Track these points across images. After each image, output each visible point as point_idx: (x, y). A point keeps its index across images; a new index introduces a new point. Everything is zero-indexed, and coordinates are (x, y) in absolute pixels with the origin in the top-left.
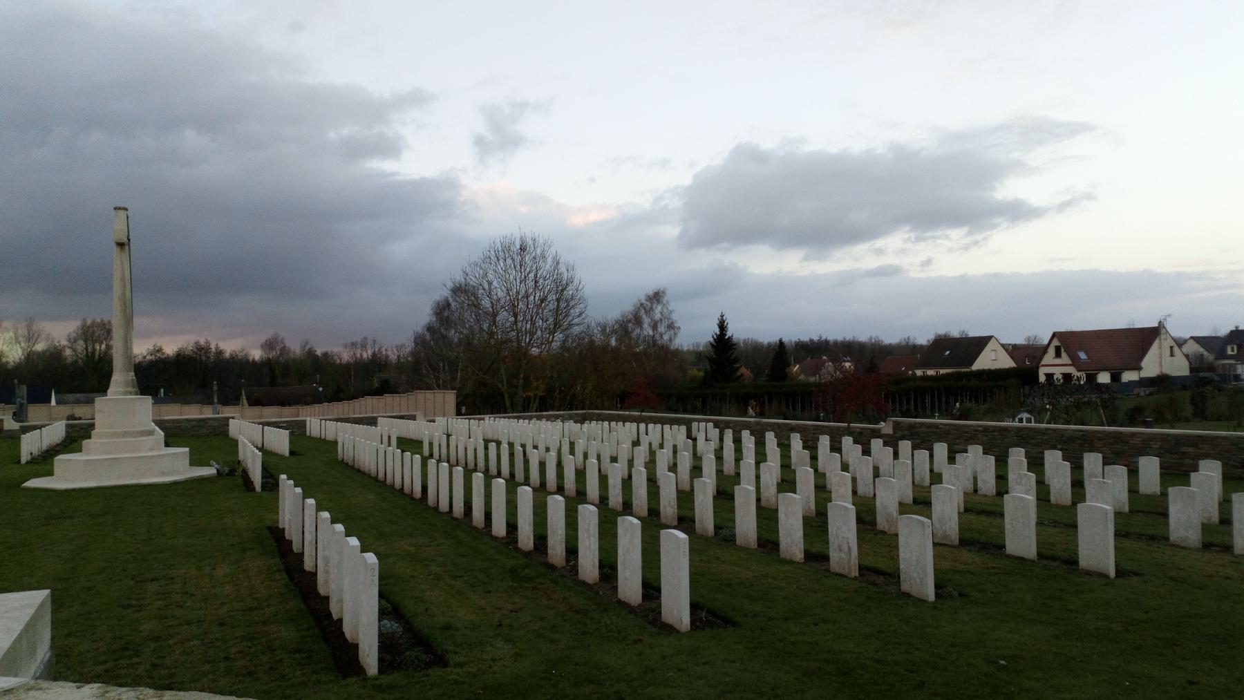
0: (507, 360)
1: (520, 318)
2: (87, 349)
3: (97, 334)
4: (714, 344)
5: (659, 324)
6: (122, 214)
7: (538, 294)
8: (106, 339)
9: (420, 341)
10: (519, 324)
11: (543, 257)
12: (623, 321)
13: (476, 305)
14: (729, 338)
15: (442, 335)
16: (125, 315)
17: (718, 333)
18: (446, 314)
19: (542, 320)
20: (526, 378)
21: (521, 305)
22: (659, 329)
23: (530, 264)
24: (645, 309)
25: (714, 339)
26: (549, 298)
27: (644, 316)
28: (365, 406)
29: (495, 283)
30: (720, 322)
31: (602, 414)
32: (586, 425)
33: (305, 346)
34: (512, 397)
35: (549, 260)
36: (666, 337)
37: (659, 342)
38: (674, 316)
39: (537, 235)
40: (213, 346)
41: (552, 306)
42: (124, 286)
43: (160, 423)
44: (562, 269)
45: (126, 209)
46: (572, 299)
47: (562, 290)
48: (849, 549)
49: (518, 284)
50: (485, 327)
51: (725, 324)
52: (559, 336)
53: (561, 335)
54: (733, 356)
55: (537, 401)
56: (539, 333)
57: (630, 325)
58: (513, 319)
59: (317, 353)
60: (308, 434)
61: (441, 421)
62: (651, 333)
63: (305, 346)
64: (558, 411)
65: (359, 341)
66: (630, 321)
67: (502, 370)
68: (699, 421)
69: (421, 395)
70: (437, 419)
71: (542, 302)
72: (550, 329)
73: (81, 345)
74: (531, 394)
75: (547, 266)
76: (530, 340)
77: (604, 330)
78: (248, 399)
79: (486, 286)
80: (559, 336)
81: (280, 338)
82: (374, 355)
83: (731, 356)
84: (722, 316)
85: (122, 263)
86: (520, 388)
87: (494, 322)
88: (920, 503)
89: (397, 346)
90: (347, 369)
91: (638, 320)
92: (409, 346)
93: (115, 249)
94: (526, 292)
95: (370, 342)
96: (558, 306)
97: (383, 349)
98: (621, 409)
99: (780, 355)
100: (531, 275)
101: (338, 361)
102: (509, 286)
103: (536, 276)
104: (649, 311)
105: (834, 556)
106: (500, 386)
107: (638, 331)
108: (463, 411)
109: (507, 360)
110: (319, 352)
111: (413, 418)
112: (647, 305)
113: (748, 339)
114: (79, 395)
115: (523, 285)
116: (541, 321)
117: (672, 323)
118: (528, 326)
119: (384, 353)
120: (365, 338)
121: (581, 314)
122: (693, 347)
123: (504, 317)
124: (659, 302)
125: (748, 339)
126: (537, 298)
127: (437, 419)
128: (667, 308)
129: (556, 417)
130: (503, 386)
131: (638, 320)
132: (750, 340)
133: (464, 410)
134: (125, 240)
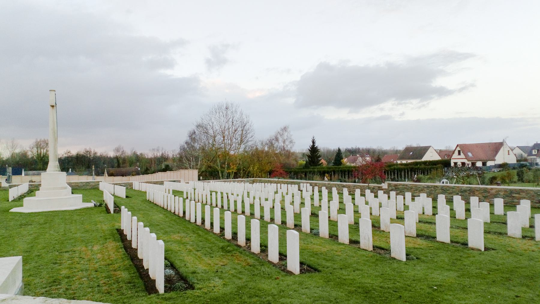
0: (220, 156)
1: (226, 138)
2: (38, 152)
4: (310, 149)
5: (286, 141)
7: (233, 128)
8: (46, 147)
9: (183, 149)
10: (225, 141)
14: (316, 147)
17: (312, 145)
18: (193, 136)
20: (228, 164)
21: (227, 133)
22: (286, 143)
26: (238, 130)
27: (280, 137)
28: (159, 176)
29: (215, 123)
31: (261, 180)
35: (238, 113)
36: (289, 146)
41: (240, 133)
47: (244, 126)
48: (369, 238)
49: (225, 123)
50: (211, 142)
53: (244, 146)
54: (318, 155)
55: (233, 174)
56: (234, 144)
60: (134, 189)
61: (191, 183)
62: (283, 145)
63: (132, 150)
67: (218, 161)
68: (303, 183)
69: (183, 172)
71: (235, 131)
73: (35, 149)
74: (230, 171)
76: (230, 148)
78: (108, 173)
79: (211, 124)
82: (162, 154)
83: (318, 154)
86: (226, 168)
87: (215, 140)
88: (399, 219)
89: (172, 150)
90: (150, 161)
94: (228, 127)
96: (242, 133)
100: (231, 120)
101: (147, 157)
102: (221, 124)
106: (217, 167)
107: (277, 144)
110: (138, 153)
111: (179, 181)
114: (34, 172)
118: (229, 142)
119: (167, 153)
120: (159, 147)
123: (219, 138)
126: (233, 129)
129: (242, 181)
130: (218, 168)
131: (277, 139)
133: (201, 178)
134: (54, 104)
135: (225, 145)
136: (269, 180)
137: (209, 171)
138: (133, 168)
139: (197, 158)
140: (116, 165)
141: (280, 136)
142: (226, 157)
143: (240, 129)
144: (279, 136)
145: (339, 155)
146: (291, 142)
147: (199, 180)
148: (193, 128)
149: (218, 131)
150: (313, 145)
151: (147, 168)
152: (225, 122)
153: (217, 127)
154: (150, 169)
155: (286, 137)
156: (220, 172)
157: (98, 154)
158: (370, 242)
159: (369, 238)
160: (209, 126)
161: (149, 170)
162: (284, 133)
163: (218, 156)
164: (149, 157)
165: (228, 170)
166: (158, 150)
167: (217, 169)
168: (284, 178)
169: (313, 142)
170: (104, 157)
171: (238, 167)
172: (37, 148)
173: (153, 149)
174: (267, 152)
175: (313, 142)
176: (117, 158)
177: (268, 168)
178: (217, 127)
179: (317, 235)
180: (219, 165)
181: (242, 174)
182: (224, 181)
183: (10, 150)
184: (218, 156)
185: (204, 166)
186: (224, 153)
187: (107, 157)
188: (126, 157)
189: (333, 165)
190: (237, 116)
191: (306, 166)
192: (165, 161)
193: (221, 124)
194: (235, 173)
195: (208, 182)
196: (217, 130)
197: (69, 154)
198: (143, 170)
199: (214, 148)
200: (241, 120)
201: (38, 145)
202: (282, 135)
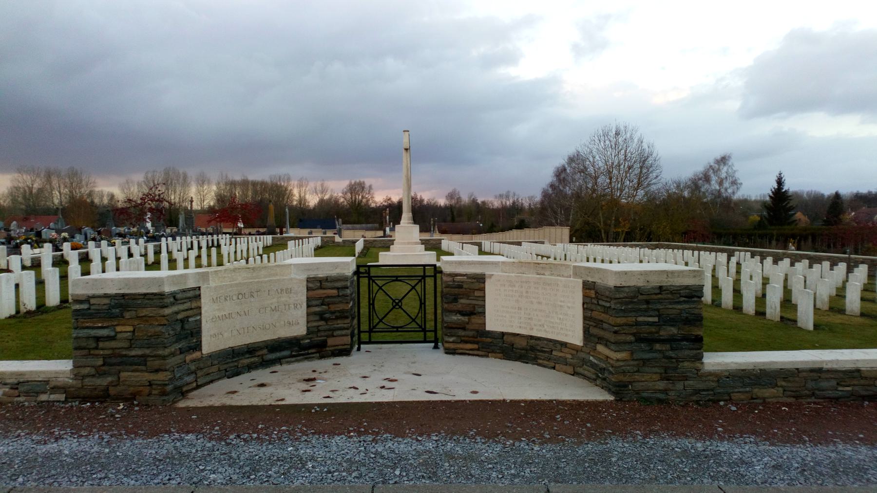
0: (604, 208)
1: (614, 180)
3: (357, 189)
5: (724, 181)
6: (407, 133)
7: (627, 164)
8: (362, 192)
9: (545, 194)
10: (613, 184)
11: (631, 138)
12: (695, 180)
13: (584, 170)
14: (786, 191)
17: (776, 187)
18: (563, 175)
19: (629, 181)
20: (617, 220)
21: (615, 172)
22: (725, 185)
23: (622, 144)
24: (713, 170)
25: (773, 192)
26: (635, 166)
27: (712, 175)
28: (515, 235)
29: (597, 157)
30: (779, 179)
31: (670, 245)
32: (655, 251)
34: (607, 233)
35: (636, 140)
36: (730, 191)
37: (724, 195)
38: (737, 175)
39: (627, 124)
40: (419, 197)
41: (637, 171)
42: (408, 170)
43: (420, 240)
44: (645, 146)
45: (408, 131)
46: (651, 166)
48: (775, 307)
49: (613, 157)
50: (590, 185)
51: (783, 180)
52: (641, 193)
53: (642, 191)
54: (789, 205)
55: (624, 235)
56: (627, 190)
57: (701, 181)
58: (609, 181)
59: (478, 201)
60: (483, 250)
61: (560, 245)
62: (718, 188)
64: (638, 242)
65: (505, 193)
66: (700, 179)
67: (601, 215)
68: (740, 251)
69: (547, 230)
71: (629, 169)
74: (620, 230)
76: (620, 195)
77: (678, 186)
78: (438, 230)
79: (591, 159)
80: (641, 193)
82: (514, 203)
83: (786, 204)
84: (780, 174)
86: (612, 226)
87: (596, 183)
88: (865, 300)
89: (529, 197)
91: (707, 178)
92: (538, 198)
93: (404, 151)
94: (619, 163)
95: (511, 195)
96: (641, 172)
97: (520, 199)
98: (687, 242)
99: (836, 203)
100: (623, 152)
101: (492, 207)
103: (626, 151)
104: (716, 171)
105: (768, 311)
106: (599, 224)
107: (706, 186)
108: (574, 240)
109: (604, 208)
110: (479, 201)
111: (543, 243)
112: (715, 167)
114: (348, 225)
117: (736, 180)
118: (619, 185)
119: (520, 201)
120: (508, 192)
121: (657, 177)
122: (761, 197)
123: (603, 180)
124: (725, 164)
128: (732, 169)
129: (636, 246)
132: (813, 193)
133: (574, 239)
134: (408, 148)
135: (612, 191)
139: (567, 210)
140: (449, 218)
143: (637, 165)
144: (711, 172)
149: (602, 168)
152: (613, 155)
155: (725, 174)
159: (775, 307)
161: (495, 226)
162: (721, 167)
163: (601, 208)
165: (615, 229)
166: (507, 197)
174: (687, 201)
179: (719, 305)
182: (608, 245)
183: (319, 195)
184: (601, 208)
187: (437, 206)
190: (633, 147)
191: (760, 225)
194: (627, 233)
195: (584, 245)
199: (594, 195)
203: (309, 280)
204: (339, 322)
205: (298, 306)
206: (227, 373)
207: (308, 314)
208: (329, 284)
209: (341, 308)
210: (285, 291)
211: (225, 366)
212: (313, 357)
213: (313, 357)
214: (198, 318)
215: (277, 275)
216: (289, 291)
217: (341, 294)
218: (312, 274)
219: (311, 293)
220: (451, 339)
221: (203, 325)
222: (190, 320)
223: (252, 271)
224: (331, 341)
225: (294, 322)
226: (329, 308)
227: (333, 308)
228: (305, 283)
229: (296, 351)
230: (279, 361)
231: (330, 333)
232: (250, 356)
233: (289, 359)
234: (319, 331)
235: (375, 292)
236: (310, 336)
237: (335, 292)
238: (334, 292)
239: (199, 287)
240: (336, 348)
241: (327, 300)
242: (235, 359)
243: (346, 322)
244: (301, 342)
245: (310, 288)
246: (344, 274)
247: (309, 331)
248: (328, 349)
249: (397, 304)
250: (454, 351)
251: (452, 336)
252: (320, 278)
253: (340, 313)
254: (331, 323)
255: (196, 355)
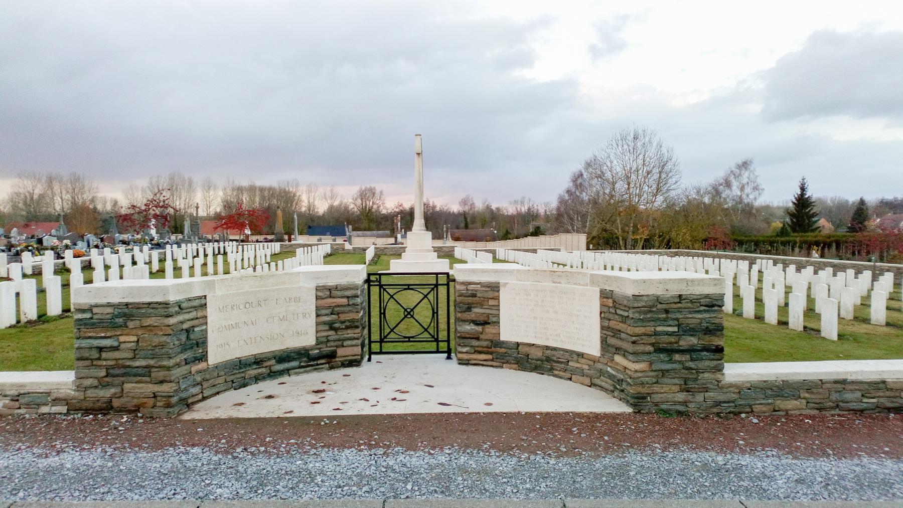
0: (621, 214)
1: (632, 185)
2: (362, 204)
4: (796, 202)
5: (746, 186)
7: (645, 169)
8: (372, 198)
9: (562, 201)
10: (631, 190)
12: (716, 185)
13: (601, 176)
14: (809, 197)
15: (577, 196)
16: (420, 190)
17: (799, 193)
18: (579, 181)
20: (635, 226)
21: (633, 177)
23: (640, 149)
24: (734, 175)
25: (796, 198)
27: (733, 181)
28: (530, 242)
29: (615, 162)
31: (690, 252)
33: (485, 202)
34: (625, 240)
35: (655, 145)
36: (751, 197)
38: (759, 181)
39: (646, 128)
41: (656, 176)
42: (420, 175)
45: (420, 135)
47: (663, 166)
48: (798, 317)
49: (631, 162)
50: (607, 191)
52: (660, 198)
53: (661, 197)
55: (642, 242)
56: (645, 195)
57: (721, 187)
58: (627, 186)
59: (492, 207)
60: (497, 258)
61: (576, 253)
62: (739, 193)
63: (485, 202)
65: (520, 199)
68: (762, 259)
69: (563, 237)
70: (574, 252)
71: (648, 174)
72: (653, 193)
73: (359, 201)
74: (638, 237)
75: (652, 152)
76: (639, 201)
77: (698, 192)
79: (609, 164)
81: (470, 198)
82: (529, 209)
83: (810, 211)
84: (803, 180)
85: (419, 163)
86: (630, 233)
87: (614, 189)
88: (890, 310)
89: (544, 203)
90: (511, 219)
92: (554, 204)
94: (637, 168)
95: (526, 201)
96: (660, 177)
97: (535, 205)
100: (641, 157)
101: (506, 214)
102: (625, 164)
110: (494, 207)
111: (559, 250)
112: (736, 172)
113: (836, 197)
114: (359, 232)
115: (635, 162)
116: (647, 187)
118: (638, 191)
119: (536, 207)
120: (524, 198)
122: (783, 203)
123: (621, 186)
125: (836, 197)
126: (645, 171)
127: (574, 252)
129: (655, 253)
130: (618, 232)
131: (728, 184)
135: (630, 197)
136: (702, 253)
137: (604, 238)
138: (486, 231)
139: (584, 216)
140: (463, 225)
141: (735, 178)
142: (630, 215)
143: (656, 170)
144: (732, 178)
145: (861, 212)
146: (755, 188)
147: (588, 249)
148: (578, 166)
149: (620, 174)
150: (802, 195)
151: (507, 231)
152: (631, 159)
153: (618, 169)
154: (511, 232)
155: (747, 179)
156: (621, 238)
157: (438, 209)
158: (800, 321)
159: (798, 317)
160: (605, 168)
161: (510, 233)
162: (743, 172)
163: (619, 214)
164: (509, 214)
165: (633, 236)
166: (522, 203)
167: (616, 234)
168: (734, 250)
169: (803, 189)
170: (446, 212)
171: (651, 232)
172: (362, 199)
173: (515, 201)
174: (707, 207)
175: (803, 189)
176: (464, 215)
177: (702, 235)
178: (618, 169)
180: (620, 228)
181: (657, 242)
182: (626, 252)
183: (329, 201)
184: (619, 214)
185: (596, 229)
186: (629, 209)
187: (450, 212)
188: (476, 214)
189: (848, 232)
191: (783, 232)
192: (533, 220)
193: (625, 164)
194: (646, 240)
195: (602, 253)
196: (617, 173)
197: (401, 208)
198: (501, 234)
199: (612, 201)
200: (658, 156)
201: (364, 195)
202: (737, 177)
203: (318, 289)
204: (349, 331)
205: (307, 316)
206: (234, 385)
207: (317, 324)
208: (339, 293)
209: (351, 318)
210: (293, 300)
211: (232, 378)
212: (323, 368)
213: (323, 368)
214: (204, 327)
215: (285, 283)
216: (298, 300)
217: (351, 303)
218: (322, 283)
219: (321, 302)
220: (465, 350)
221: (209, 335)
222: (196, 329)
223: (259, 279)
224: (340, 352)
225: (303, 332)
226: (339, 317)
227: (343, 317)
228: (314, 291)
229: (305, 362)
230: (287, 372)
231: (340, 343)
232: (257, 367)
233: (297, 370)
234: (328, 341)
235: (386, 301)
236: (319, 346)
237: (345, 301)
238: (344, 301)
239: (205, 296)
240: (347, 358)
241: (336, 309)
242: (242, 370)
243: (355, 332)
244: (310, 353)
245: (319, 296)
246: (354, 282)
247: (318, 342)
248: (337, 359)
249: (409, 313)
250: (467, 362)
251: (465, 346)
252: (330, 286)
253: (350, 322)
254: (341, 333)
255: (202, 366)
